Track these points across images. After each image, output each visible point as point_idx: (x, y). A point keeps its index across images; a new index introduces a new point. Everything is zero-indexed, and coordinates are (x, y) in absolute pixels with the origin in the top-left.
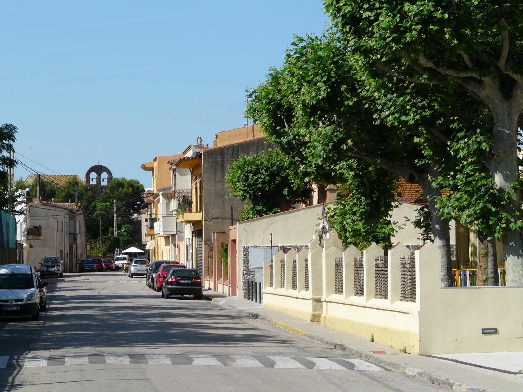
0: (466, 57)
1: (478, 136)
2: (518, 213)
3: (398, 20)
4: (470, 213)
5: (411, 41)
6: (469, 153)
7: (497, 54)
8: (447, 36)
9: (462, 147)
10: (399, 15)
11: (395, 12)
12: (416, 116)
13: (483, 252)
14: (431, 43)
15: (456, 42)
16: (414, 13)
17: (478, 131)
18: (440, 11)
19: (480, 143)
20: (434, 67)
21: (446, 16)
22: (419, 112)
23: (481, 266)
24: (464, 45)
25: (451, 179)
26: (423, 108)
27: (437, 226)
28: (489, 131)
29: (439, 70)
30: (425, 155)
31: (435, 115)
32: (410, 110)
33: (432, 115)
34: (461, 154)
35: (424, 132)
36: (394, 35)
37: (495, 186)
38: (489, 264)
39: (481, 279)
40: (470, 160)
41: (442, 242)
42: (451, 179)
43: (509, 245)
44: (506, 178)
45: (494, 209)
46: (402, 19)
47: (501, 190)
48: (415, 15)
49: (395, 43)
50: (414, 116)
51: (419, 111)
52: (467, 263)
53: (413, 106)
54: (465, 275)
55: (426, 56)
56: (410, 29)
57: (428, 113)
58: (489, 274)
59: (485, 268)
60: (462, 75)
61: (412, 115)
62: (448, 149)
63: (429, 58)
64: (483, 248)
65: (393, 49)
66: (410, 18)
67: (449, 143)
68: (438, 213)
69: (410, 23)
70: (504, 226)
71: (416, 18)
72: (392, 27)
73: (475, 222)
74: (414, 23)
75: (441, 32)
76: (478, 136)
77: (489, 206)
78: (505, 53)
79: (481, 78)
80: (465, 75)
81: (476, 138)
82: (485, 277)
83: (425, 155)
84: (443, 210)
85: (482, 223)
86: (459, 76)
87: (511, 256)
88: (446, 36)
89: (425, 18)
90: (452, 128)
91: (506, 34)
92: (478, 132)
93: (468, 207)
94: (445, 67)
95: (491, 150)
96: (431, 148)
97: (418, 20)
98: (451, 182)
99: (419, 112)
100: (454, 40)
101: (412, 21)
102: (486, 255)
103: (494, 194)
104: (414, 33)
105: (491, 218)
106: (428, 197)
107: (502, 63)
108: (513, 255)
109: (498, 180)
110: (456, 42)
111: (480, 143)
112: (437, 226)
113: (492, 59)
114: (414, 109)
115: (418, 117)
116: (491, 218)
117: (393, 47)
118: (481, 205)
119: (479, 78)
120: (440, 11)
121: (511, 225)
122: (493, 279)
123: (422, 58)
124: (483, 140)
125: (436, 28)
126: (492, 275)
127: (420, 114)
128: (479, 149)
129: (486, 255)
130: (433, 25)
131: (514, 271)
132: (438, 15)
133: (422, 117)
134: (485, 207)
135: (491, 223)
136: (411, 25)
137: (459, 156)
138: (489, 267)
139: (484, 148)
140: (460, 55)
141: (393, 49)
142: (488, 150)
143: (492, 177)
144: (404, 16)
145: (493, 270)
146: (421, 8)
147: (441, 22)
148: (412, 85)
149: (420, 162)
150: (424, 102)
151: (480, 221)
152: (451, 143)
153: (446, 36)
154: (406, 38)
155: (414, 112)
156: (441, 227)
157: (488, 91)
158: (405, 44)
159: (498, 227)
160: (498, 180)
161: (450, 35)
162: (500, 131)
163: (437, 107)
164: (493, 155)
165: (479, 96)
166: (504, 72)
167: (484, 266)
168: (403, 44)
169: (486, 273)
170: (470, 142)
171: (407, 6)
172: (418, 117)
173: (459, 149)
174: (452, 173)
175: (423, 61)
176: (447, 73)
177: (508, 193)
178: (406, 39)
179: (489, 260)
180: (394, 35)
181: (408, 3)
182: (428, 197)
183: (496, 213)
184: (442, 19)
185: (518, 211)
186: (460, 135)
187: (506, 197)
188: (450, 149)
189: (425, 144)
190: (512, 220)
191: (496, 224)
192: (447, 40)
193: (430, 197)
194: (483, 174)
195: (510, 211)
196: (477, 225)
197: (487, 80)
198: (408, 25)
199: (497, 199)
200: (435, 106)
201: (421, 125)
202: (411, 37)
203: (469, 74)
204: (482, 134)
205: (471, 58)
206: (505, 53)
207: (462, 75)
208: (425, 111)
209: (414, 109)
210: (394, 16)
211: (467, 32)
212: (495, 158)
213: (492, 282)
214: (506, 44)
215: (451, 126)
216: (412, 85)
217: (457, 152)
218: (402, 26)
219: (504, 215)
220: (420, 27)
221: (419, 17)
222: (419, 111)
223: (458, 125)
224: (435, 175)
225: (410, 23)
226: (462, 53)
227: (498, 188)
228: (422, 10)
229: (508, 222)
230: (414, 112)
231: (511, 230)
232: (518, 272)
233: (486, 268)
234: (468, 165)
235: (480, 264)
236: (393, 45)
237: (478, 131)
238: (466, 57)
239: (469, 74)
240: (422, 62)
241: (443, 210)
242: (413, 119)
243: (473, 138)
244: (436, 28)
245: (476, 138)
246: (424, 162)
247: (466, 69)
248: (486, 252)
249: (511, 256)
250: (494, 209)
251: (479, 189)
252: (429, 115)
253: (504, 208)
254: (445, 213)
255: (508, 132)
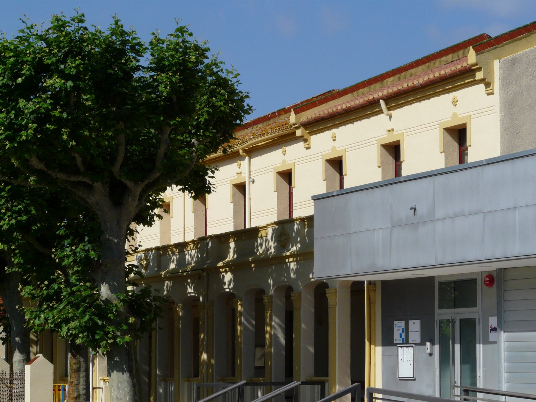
0: (79, 160)
1: (85, 244)
2: (125, 327)
3: (13, 117)
4: (75, 326)
5: (27, 139)
6: (75, 261)
7: (113, 160)
8: (65, 137)
9: (67, 253)
10: (13, 112)
11: (9, 108)
12: (11, 220)
13: (75, 367)
14: (46, 143)
15: (74, 143)
16: (31, 110)
17: (87, 239)
18: (59, 110)
19: (88, 251)
20: (45, 169)
21: (65, 115)
22: (14, 217)
23: (72, 382)
24: (81, 147)
25: (45, 288)
26: (19, 213)
27: (17, 339)
28: (97, 240)
29: (50, 172)
30: (15, 262)
31: (32, 221)
32: (5, 214)
33: (28, 220)
34: (66, 262)
35: (20, 238)
36: (8, 132)
37: (101, 297)
38: (81, 380)
39: (72, 396)
40: (75, 269)
41: (22, 356)
42: (45, 288)
43: (113, 360)
44: (112, 289)
45: (100, 323)
46: (17, 116)
47: (107, 302)
48: (31, 113)
49: (9, 142)
50: (9, 221)
51: (14, 216)
52: (65, 378)
53: (7, 209)
54: (65, 390)
55: (38, 157)
56: (26, 128)
57: (24, 218)
58: (81, 391)
59: (77, 385)
60: (73, 179)
61: (7, 219)
62: (53, 256)
63: (41, 159)
64: (75, 363)
65: (7, 147)
66: (26, 116)
67: (54, 250)
68: (28, 325)
69: (25, 121)
70: (112, 341)
71: (32, 116)
72: (6, 124)
73: (80, 335)
74: (31, 122)
75: (57, 133)
76: (85, 244)
77: (96, 319)
78: (120, 158)
79: (93, 183)
80: (76, 180)
81: (84, 246)
82: (76, 394)
83: (15, 262)
84: (34, 322)
85: (88, 336)
86: (70, 180)
87: (115, 372)
88: (64, 137)
89: (41, 116)
90: (59, 234)
91: (122, 138)
92: (86, 240)
93: (72, 319)
94: (57, 170)
95: (99, 260)
96: (22, 255)
97: (34, 118)
98: (45, 292)
99: (14, 217)
100: (72, 141)
101: (28, 119)
102: (78, 371)
103: (100, 305)
104: (30, 131)
105: (98, 332)
106: (17, 307)
107: (116, 169)
108: (118, 371)
109: (104, 291)
110: (74, 143)
111: (88, 251)
112: (17, 339)
113: (107, 164)
114: (9, 213)
115: (13, 221)
116: (98, 332)
117: (7, 145)
118: (87, 317)
119: (91, 183)
120: (59, 110)
121: (118, 340)
122: (85, 396)
123: (34, 159)
124: (91, 248)
125: (53, 127)
126: (84, 392)
127: (16, 218)
128: (87, 258)
129: (78, 371)
130: (49, 125)
131: (118, 388)
132: (57, 113)
133: (17, 222)
134: (90, 319)
135: (97, 337)
136: (27, 123)
137: (64, 264)
138: (81, 384)
139: (92, 257)
140: (74, 158)
141: (7, 147)
142: (96, 259)
143: (98, 286)
144: (19, 113)
145: (85, 387)
146: (38, 106)
147: (60, 122)
148: (9, 187)
149: (10, 270)
150: (20, 206)
151: (85, 334)
152: (56, 250)
153: (64, 137)
154: (21, 136)
155: (9, 217)
156: (22, 340)
157: (98, 197)
158: (21, 143)
159: (105, 342)
160: (104, 291)
161: (68, 136)
162: (108, 240)
163: (33, 212)
164: (101, 264)
165: (87, 202)
166: (118, 178)
167: (76, 382)
168: (18, 143)
169: (78, 389)
170: (78, 250)
171: (22, 103)
172: (13, 221)
173: (64, 256)
174: (46, 283)
175: (35, 162)
176: (58, 176)
177: (116, 306)
178: (21, 137)
179: (81, 376)
180: (8, 132)
181: (22, 100)
182: (17, 307)
183: (103, 327)
184: (60, 119)
185: (125, 325)
186: (66, 243)
187: (114, 310)
188: (55, 257)
189: (17, 251)
190: (119, 334)
191: (102, 339)
192: (64, 141)
193: (19, 308)
194: (88, 284)
195: (118, 325)
196: (82, 339)
197: (97, 185)
198: (23, 123)
199: (102, 310)
200: (31, 211)
201: (15, 230)
202: (27, 136)
203: (81, 179)
204: (89, 242)
205: (83, 162)
206: (120, 158)
207: (73, 179)
208: (20, 216)
209: (9, 213)
210: (8, 112)
211: (85, 133)
212: (103, 268)
213: (84, 399)
214: (122, 148)
215: (58, 232)
216: (9, 187)
217: (62, 259)
218: (16, 123)
219: (110, 329)
220: (35, 125)
221: (35, 115)
222: (14, 216)
223: (65, 231)
224: (25, 283)
225: (25, 121)
226: (76, 155)
227: (103, 299)
228: (40, 107)
229: (115, 337)
230: (9, 217)
231: (118, 344)
232: (123, 389)
233: (78, 384)
234: (73, 274)
235: (72, 380)
236: (7, 143)
237: (87, 239)
238: (79, 160)
239: (81, 179)
240: (34, 163)
241: (34, 322)
242: (8, 224)
243: (81, 246)
244: (53, 127)
245: (84, 246)
246: (14, 269)
247: (77, 172)
248: (78, 368)
249: (115, 372)
250: (100, 323)
251: (84, 300)
252: (25, 220)
253: (110, 322)
254: (36, 324)
255: (116, 241)
